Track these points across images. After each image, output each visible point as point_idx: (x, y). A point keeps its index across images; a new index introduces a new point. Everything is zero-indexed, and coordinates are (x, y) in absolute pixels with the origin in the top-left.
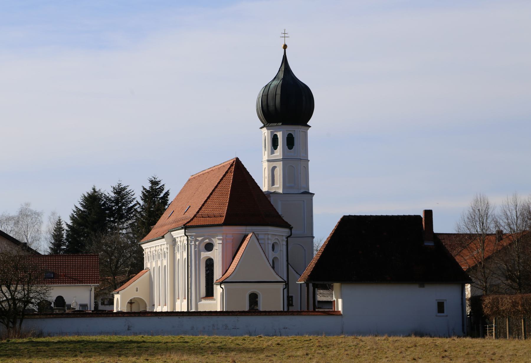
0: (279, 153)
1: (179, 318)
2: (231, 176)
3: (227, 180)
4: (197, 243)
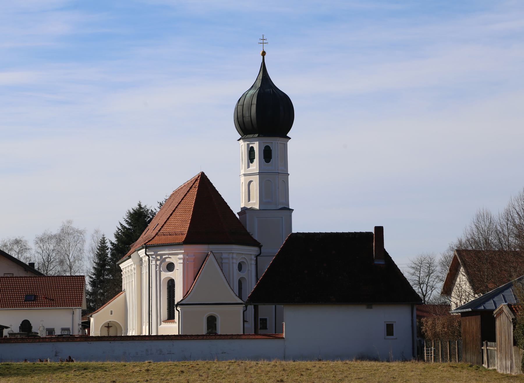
0: (255, 167)
1: (110, 343)
2: (195, 191)
3: (191, 196)
4: (158, 263)
